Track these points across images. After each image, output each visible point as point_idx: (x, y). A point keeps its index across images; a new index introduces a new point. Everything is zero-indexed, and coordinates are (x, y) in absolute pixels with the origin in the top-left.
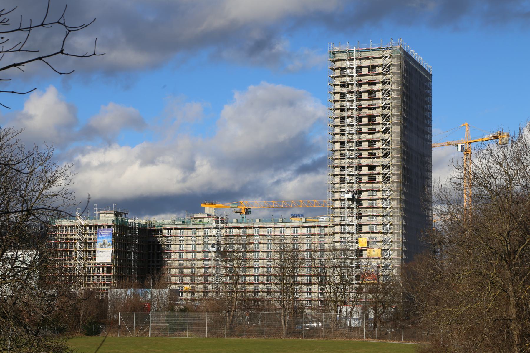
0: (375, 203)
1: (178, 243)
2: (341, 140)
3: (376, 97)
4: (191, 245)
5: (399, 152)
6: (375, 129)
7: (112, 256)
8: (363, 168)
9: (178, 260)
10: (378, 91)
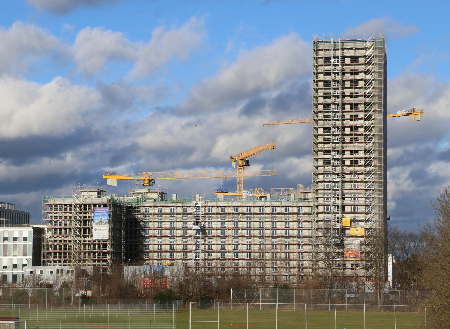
1: (156, 220)
2: (324, 125)
3: (358, 86)
4: (169, 222)
5: (381, 138)
6: (357, 116)
7: (109, 233)
9: (157, 237)
10: (362, 80)
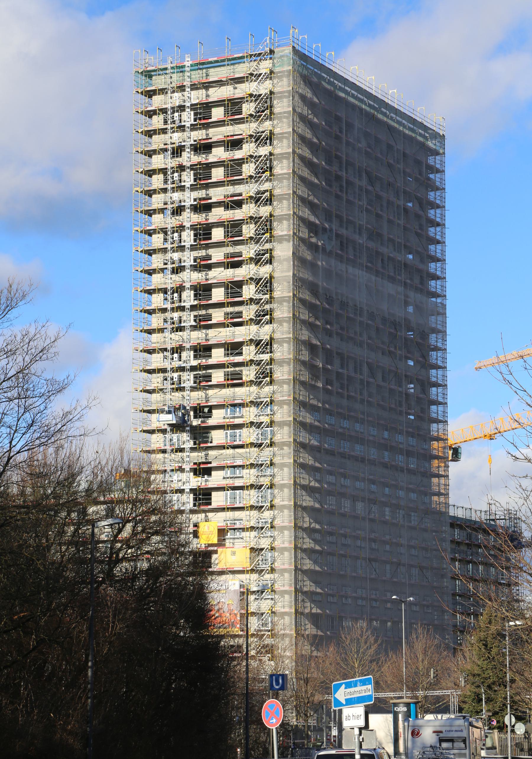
0: (240, 436)
8: (214, 351)
